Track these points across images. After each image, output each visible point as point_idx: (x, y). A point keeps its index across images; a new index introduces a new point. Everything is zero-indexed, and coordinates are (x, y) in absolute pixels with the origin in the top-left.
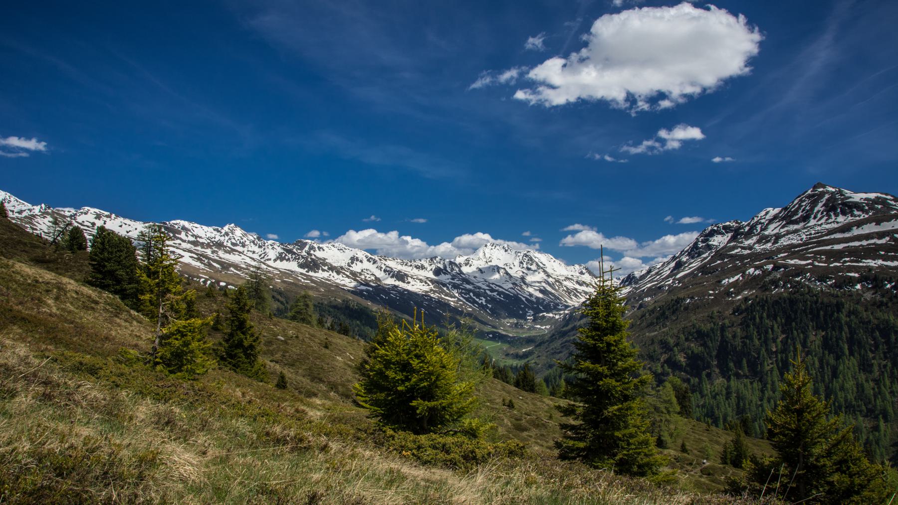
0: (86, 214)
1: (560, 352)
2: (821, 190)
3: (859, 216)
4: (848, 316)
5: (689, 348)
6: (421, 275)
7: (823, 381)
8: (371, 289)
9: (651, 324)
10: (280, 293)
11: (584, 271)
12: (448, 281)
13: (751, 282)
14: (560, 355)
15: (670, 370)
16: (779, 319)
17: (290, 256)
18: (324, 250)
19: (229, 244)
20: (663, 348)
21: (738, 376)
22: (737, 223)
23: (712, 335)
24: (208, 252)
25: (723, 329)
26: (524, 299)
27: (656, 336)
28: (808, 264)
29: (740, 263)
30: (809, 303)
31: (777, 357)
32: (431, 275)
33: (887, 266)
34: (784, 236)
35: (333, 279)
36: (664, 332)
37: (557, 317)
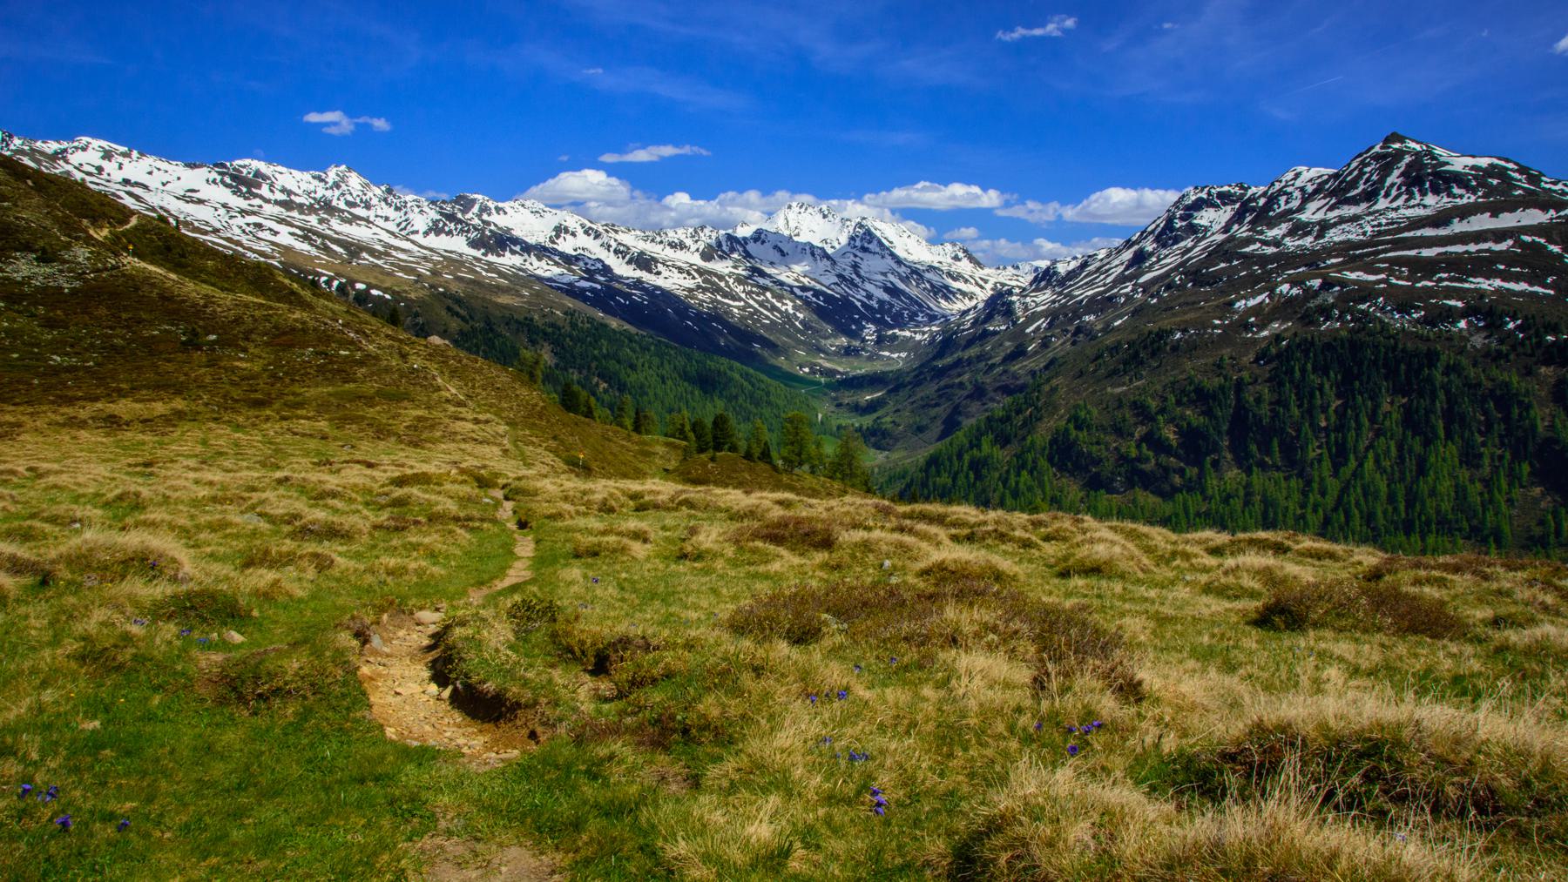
0: (84, 149)
1: (937, 405)
2: (1397, 146)
3: (1461, 197)
4: (1446, 373)
5: (1183, 417)
6: (680, 260)
7: (1402, 479)
8: (599, 287)
9: (1113, 373)
10: (458, 301)
11: (961, 255)
12: (726, 271)
13: (1284, 308)
14: (937, 409)
15: (1151, 454)
16: (1332, 374)
17: (452, 226)
18: (505, 213)
19: (342, 206)
20: (1137, 415)
21: (1263, 465)
22: (1242, 188)
23: (1221, 396)
24: (313, 220)
25: (1239, 386)
26: (858, 304)
27: (1125, 394)
28: (1379, 282)
29: (1263, 271)
30: (1383, 350)
31: (1328, 436)
32: (697, 260)
33: (1508, 290)
34: (1334, 225)
35: (530, 268)
36: (1138, 388)
37: (918, 337)
